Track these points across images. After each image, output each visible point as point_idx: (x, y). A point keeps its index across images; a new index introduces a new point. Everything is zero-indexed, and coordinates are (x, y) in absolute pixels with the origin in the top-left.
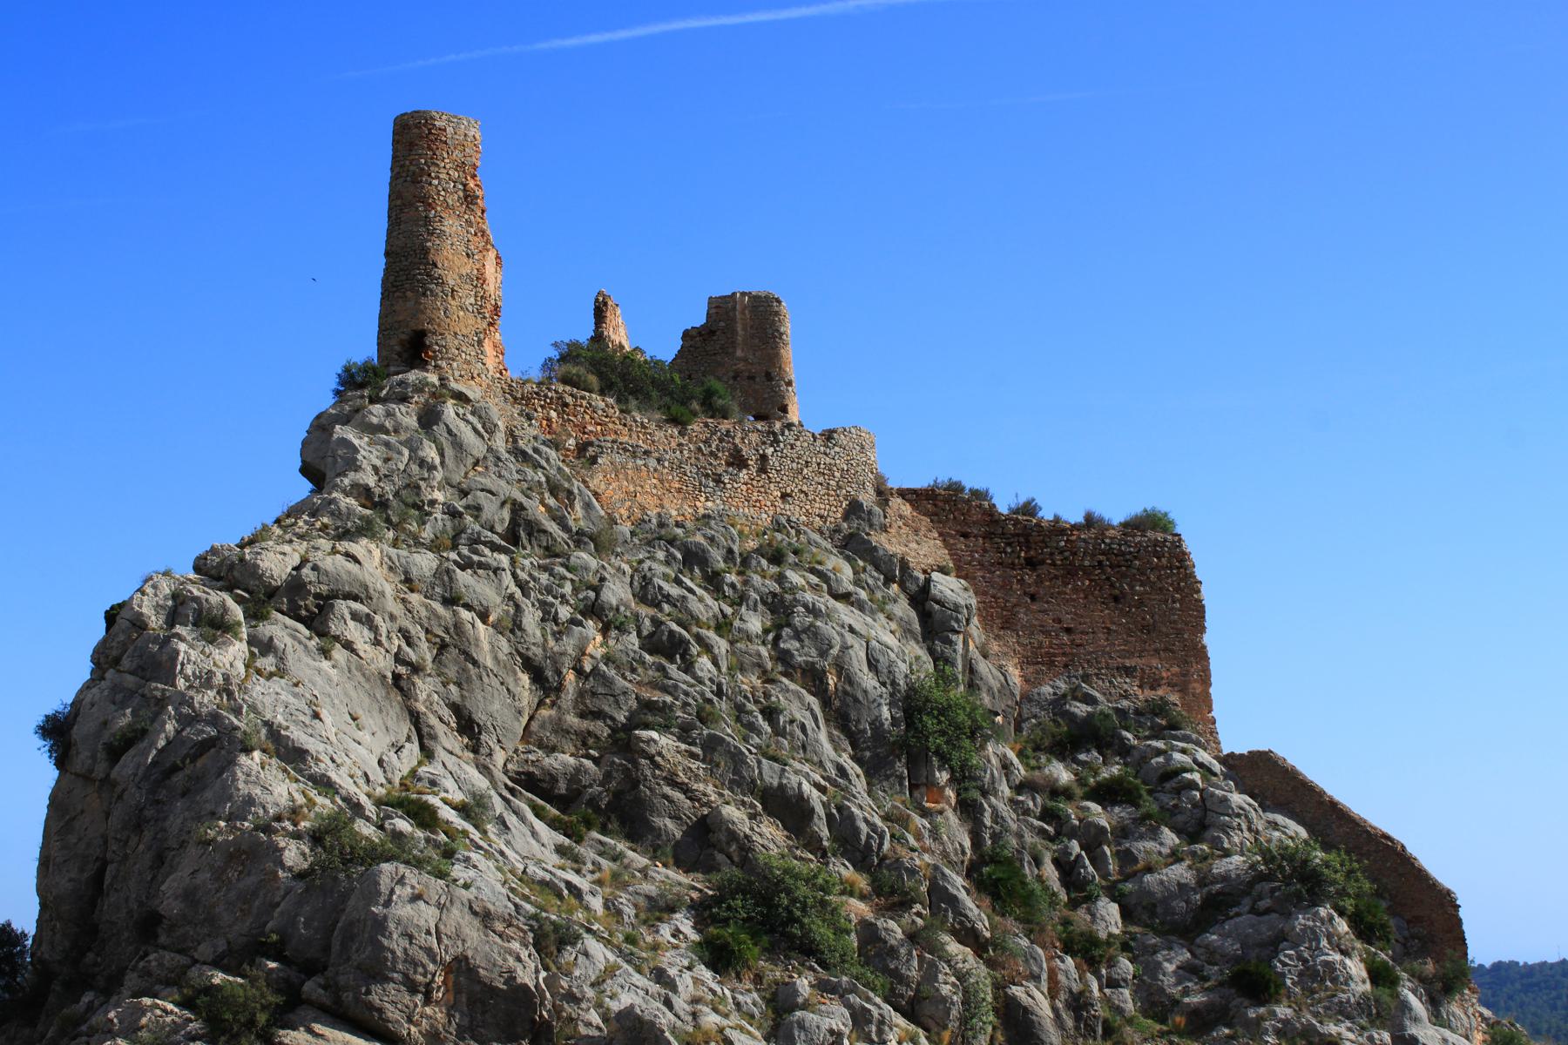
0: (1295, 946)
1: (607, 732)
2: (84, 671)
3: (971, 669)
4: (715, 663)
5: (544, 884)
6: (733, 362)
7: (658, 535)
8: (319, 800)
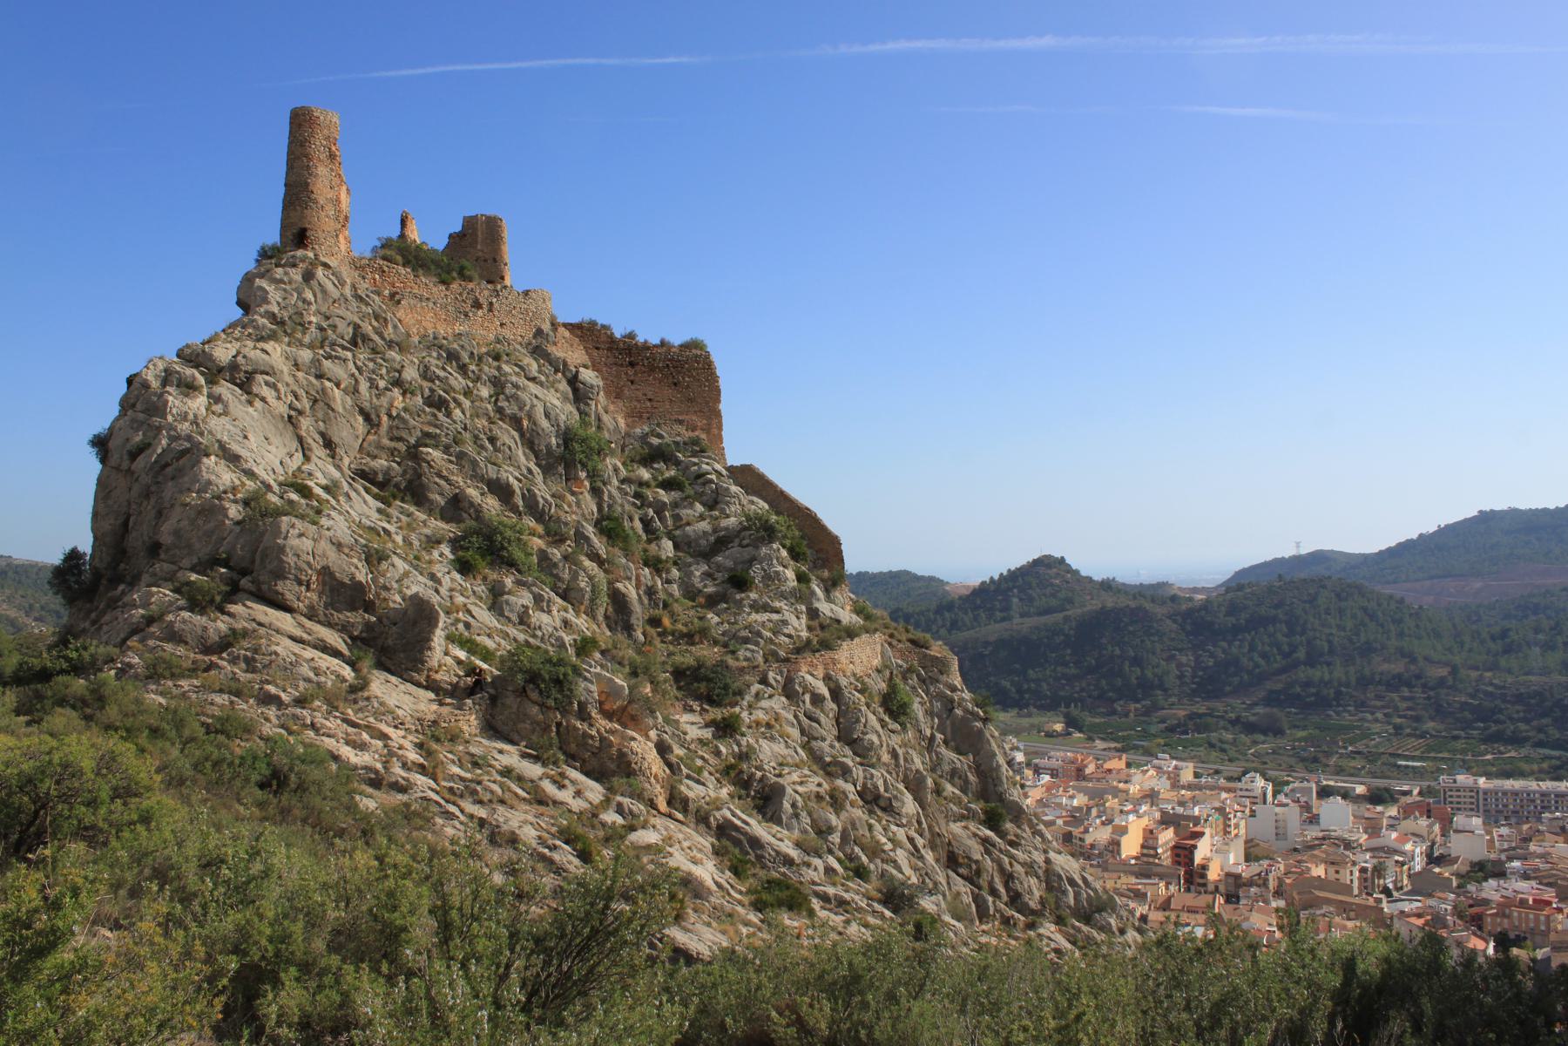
2: (115, 411)
5: (370, 528)
6: (474, 253)
7: (433, 344)
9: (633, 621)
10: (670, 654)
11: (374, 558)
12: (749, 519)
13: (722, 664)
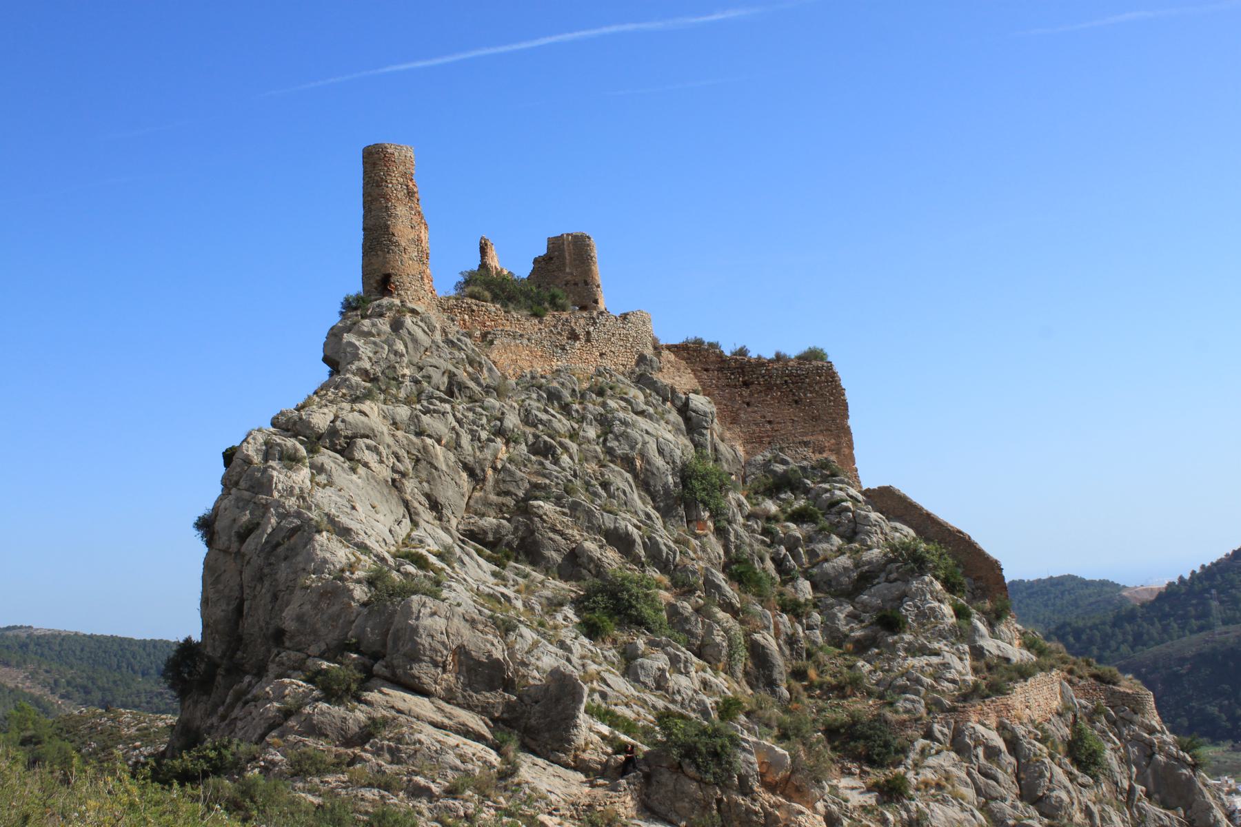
0: (912, 599)
1: (513, 503)
2: (218, 490)
3: (716, 450)
4: (571, 458)
5: (490, 596)
6: (563, 277)
7: (531, 384)
8: (362, 557)
9: (776, 675)
10: (820, 710)
11: (506, 628)
12: (893, 548)
13: (880, 718)
